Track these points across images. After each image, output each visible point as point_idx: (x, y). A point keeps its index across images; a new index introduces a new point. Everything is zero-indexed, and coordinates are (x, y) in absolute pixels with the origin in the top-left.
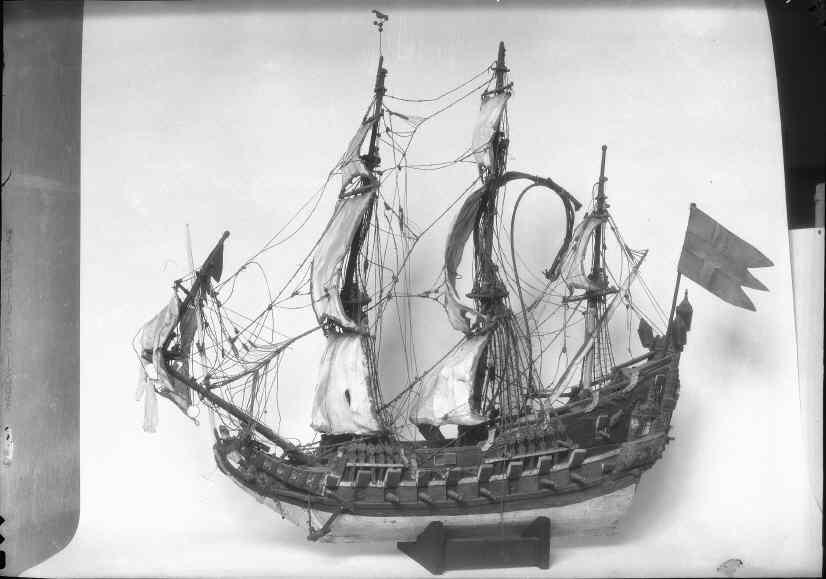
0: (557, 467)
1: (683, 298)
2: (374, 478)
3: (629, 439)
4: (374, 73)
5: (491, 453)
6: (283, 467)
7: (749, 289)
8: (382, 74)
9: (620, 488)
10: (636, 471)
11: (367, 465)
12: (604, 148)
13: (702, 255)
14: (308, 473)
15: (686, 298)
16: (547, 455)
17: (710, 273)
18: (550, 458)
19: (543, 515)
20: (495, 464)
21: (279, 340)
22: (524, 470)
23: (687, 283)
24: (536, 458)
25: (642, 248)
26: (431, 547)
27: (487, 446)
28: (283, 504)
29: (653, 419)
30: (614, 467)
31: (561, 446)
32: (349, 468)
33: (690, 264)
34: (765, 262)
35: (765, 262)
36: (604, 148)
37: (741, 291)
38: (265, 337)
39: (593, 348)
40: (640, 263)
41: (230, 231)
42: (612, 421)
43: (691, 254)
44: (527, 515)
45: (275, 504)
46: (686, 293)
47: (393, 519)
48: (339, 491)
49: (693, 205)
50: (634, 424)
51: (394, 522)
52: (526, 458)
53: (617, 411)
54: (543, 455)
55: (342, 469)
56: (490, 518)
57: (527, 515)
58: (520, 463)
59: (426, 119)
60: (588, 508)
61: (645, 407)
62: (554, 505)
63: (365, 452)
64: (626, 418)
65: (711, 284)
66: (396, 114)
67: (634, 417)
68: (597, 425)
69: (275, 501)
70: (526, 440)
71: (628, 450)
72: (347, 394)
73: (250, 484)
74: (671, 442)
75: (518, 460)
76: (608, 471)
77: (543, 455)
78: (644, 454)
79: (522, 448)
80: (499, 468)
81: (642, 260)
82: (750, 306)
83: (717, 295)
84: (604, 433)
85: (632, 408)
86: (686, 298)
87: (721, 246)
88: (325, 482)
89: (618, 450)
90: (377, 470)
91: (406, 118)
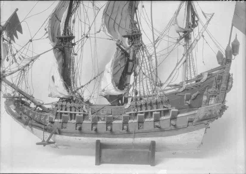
0: (163, 118)
1: (234, 38)
2: (70, 118)
3: (202, 105)
5: (128, 109)
6: (32, 112)
9: (197, 129)
10: (205, 122)
11: (66, 112)
15: (236, 38)
16: (157, 111)
18: (159, 113)
20: (130, 114)
21: (35, 55)
22: (130, 119)
24: (152, 113)
25: (212, 12)
27: (127, 106)
28: (34, 129)
29: (215, 96)
30: (53, 127)
31: (164, 107)
32: (58, 112)
38: (30, 55)
39: (185, 61)
40: (210, 20)
41: (18, 8)
42: (193, 97)
44: (147, 140)
45: (30, 129)
46: (236, 36)
47: (80, 138)
48: (55, 124)
50: (205, 98)
51: (80, 139)
52: (146, 112)
53: (196, 92)
54: (155, 111)
55: (55, 113)
57: (147, 140)
58: (143, 115)
60: (179, 139)
61: (210, 90)
62: (161, 136)
63: (66, 105)
64: (200, 95)
67: (206, 95)
68: (185, 99)
70: (151, 103)
71: (201, 112)
72: (53, 78)
73: (19, 119)
75: (142, 113)
76: (191, 121)
77: (155, 111)
78: (209, 113)
79: (144, 108)
80: (131, 116)
84: (189, 102)
85: (204, 90)
86: (236, 38)
88: (48, 119)
89: (196, 111)
90: (71, 114)
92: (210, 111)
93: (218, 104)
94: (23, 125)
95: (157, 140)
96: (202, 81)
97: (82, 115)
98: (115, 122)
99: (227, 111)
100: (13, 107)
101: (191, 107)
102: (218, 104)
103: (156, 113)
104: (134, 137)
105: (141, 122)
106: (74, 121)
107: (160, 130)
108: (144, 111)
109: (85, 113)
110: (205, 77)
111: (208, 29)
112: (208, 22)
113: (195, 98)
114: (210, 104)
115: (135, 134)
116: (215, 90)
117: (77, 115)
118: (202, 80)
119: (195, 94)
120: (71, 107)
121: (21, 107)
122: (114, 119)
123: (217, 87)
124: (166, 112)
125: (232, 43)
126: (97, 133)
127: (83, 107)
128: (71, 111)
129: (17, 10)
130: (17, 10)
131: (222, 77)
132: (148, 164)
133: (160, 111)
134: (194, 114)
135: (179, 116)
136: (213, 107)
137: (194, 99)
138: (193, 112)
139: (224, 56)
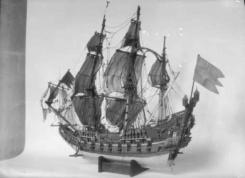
0: (143, 145)
2: (88, 141)
4: (103, 20)
7: (217, 86)
8: (104, 20)
9: (164, 154)
12: (165, 37)
13: (202, 74)
14: (144, 129)
15: (197, 89)
17: (204, 80)
18: (139, 141)
19: (134, 159)
23: (196, 84)
26: (104, 165)
33: (197, 77)
34: (222, 76)
35: (222, 76)
36: (165, 37)
37: (215, 86)
40: (177, 77)
43: (198, 73)
49: (199, 55)
52: (131, 140)
56: (120, 158)
59: (116, 33)
62: (141, 157)
65: (204, 84)
66: (108, 32)
69: (194, 125)
73: (66, 139)
74: (191, 139)
78: (170, 143)
79: (130, 137)
81: (177, 76)
82: (217, 92)
83: (207, 88)
87: (208, 70)
89: (164, 141)
90: (88, 138)
91: (110, 33)
92: (171, 141)
93: (178, 137)
94: (68, 143)
95: (138, 159)
96: (168, 120)
97: (94, 139)
98: (114, 145)
99: (191, 141)
100: (62, 131)
101: (160, 139)
102: (178, 137)
103: (137, 141)
104: (124, 156)
105: (129, 147)
106: (90, 143)
107: (139, 152)
108: (130, 139)
109: (96, 138)
110: (170, 117)
111: (148, 91)
112: (176, 78)
113: (163, 132)
114: (173, 136)
115: (124, 155)
116: (175, 127)
117: (92, 139)
118: (169, 119)
119: (163, 129)
120: (88, 134)
121: (66, 132)
122: (113, 143)
123: (178, 125)
124: (144, 141)
125: (195, 93)
126: (102, 150)
127: (95, 134)
128: (88, 136)
129: (69, 70)
130: (69, 70)
131: (181, 117)
132: (128, 175)
133: (140, 140)
134: (163, 143)
135: (153, 144)
136: (174, 140)
137: (162, 133)
138: (162, 142)
139: (189, 102)
